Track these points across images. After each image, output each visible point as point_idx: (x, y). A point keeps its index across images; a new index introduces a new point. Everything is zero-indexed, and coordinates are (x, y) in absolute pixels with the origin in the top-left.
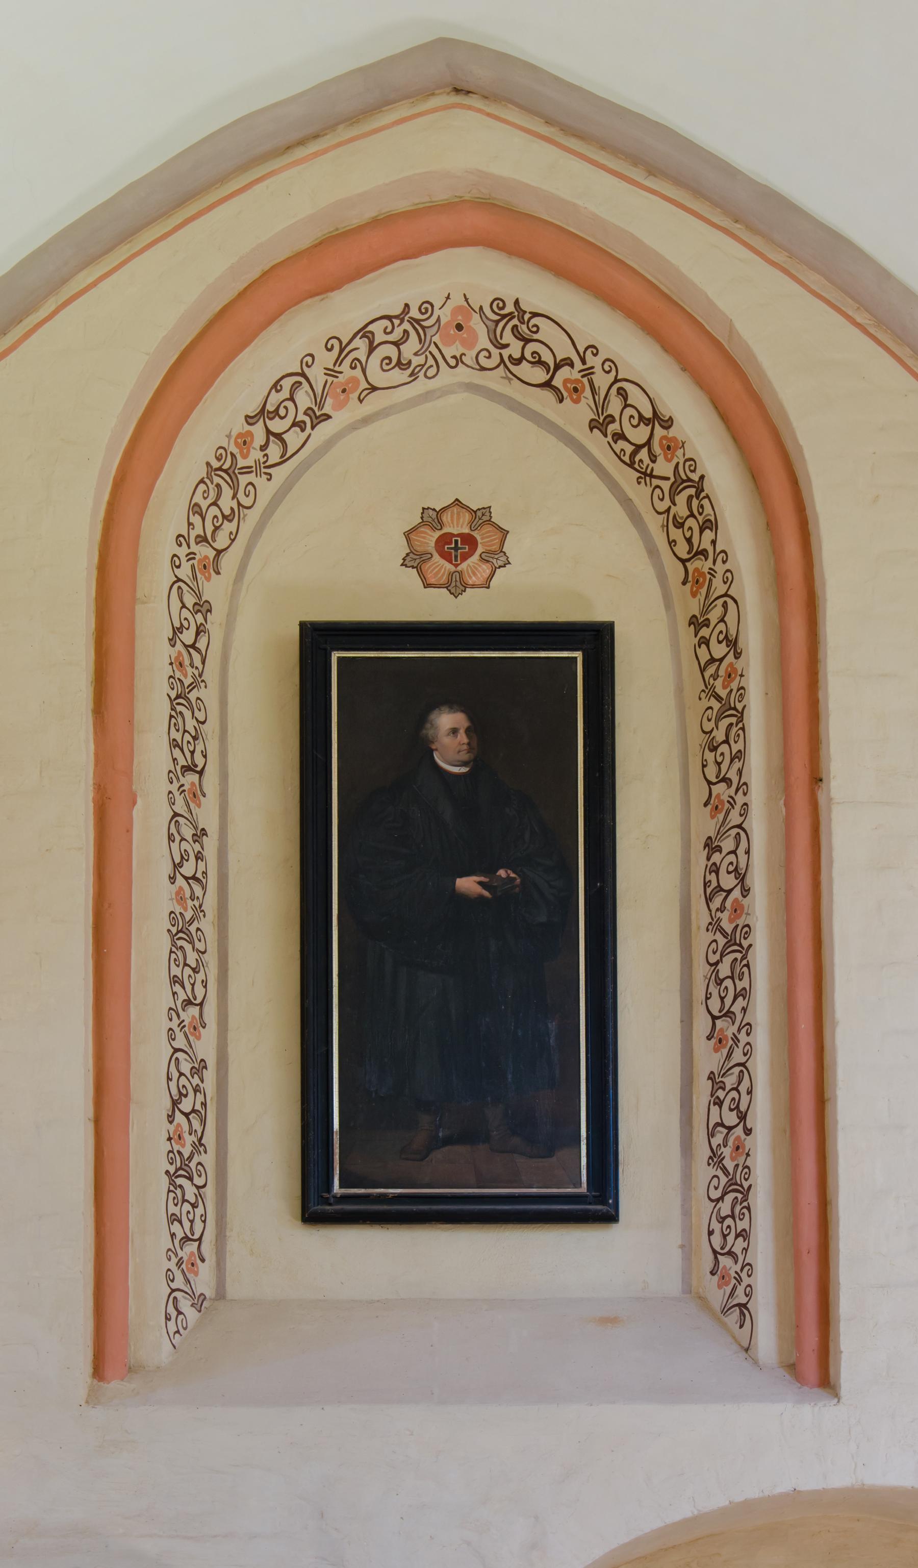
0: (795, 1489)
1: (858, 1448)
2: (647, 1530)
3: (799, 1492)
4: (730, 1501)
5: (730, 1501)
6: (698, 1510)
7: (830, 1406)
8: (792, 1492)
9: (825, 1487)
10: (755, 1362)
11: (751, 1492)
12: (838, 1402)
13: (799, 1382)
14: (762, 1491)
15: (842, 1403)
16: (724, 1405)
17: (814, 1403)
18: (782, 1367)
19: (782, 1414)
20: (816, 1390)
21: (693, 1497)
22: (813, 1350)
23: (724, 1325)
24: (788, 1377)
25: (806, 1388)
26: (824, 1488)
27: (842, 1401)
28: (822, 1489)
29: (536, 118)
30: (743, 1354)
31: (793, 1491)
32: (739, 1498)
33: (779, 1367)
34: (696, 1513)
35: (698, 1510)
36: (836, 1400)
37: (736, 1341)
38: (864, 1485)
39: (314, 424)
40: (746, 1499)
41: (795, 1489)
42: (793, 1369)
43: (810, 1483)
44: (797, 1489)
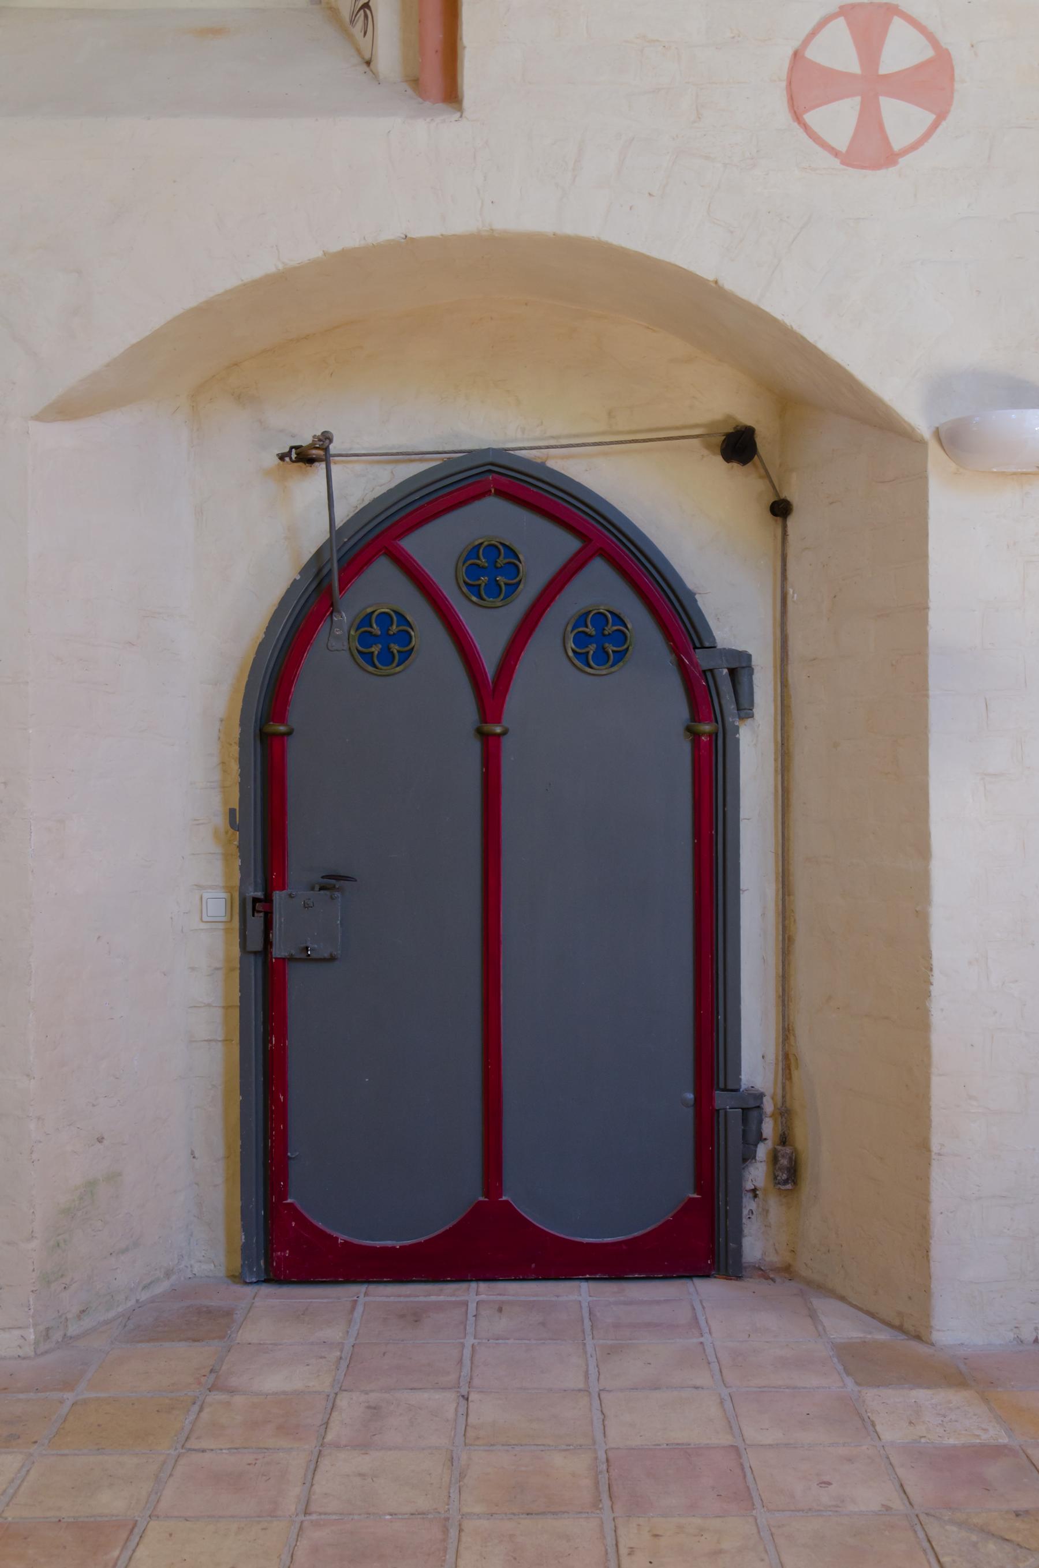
0: (406, 236)
1: (485, 180)
2: (221, 291)
3: (413, 239)
4: (324, 251)
5: (324, 251)
6: (283, 263)
7: (451, 122)
8: (403, 240)
9: (444, 233)
10: (375, 76)
11: (351, 240)
12: (461, 116)
13: (420, 96)
14: (364, 238)
15: (465, 117)
16: (317, 120)
17: (431, 118)
18: (406, 81)
19: (389, 132)
20: (441, 105)
21: (276, 246)
22: (437, 51)
23: (350, 37)
24: (410, 92)
25: (428, 104)
26: (442, 235)
27: (465, 114)
28: (441, 237)
29: (293, 690)
30: (365, 67)
31: (403, 238)
32: (335, 247)
33: (403, 82)
34: (281, 267)
35: (283, 263)
36: (459, 114)
37: (359, 51)
38: (492, 230)
39: (490, 661)
40: (343, 249)
41: (406, 236)
42: (416, 83)
43: (426, 228)
44: (409, 235)
